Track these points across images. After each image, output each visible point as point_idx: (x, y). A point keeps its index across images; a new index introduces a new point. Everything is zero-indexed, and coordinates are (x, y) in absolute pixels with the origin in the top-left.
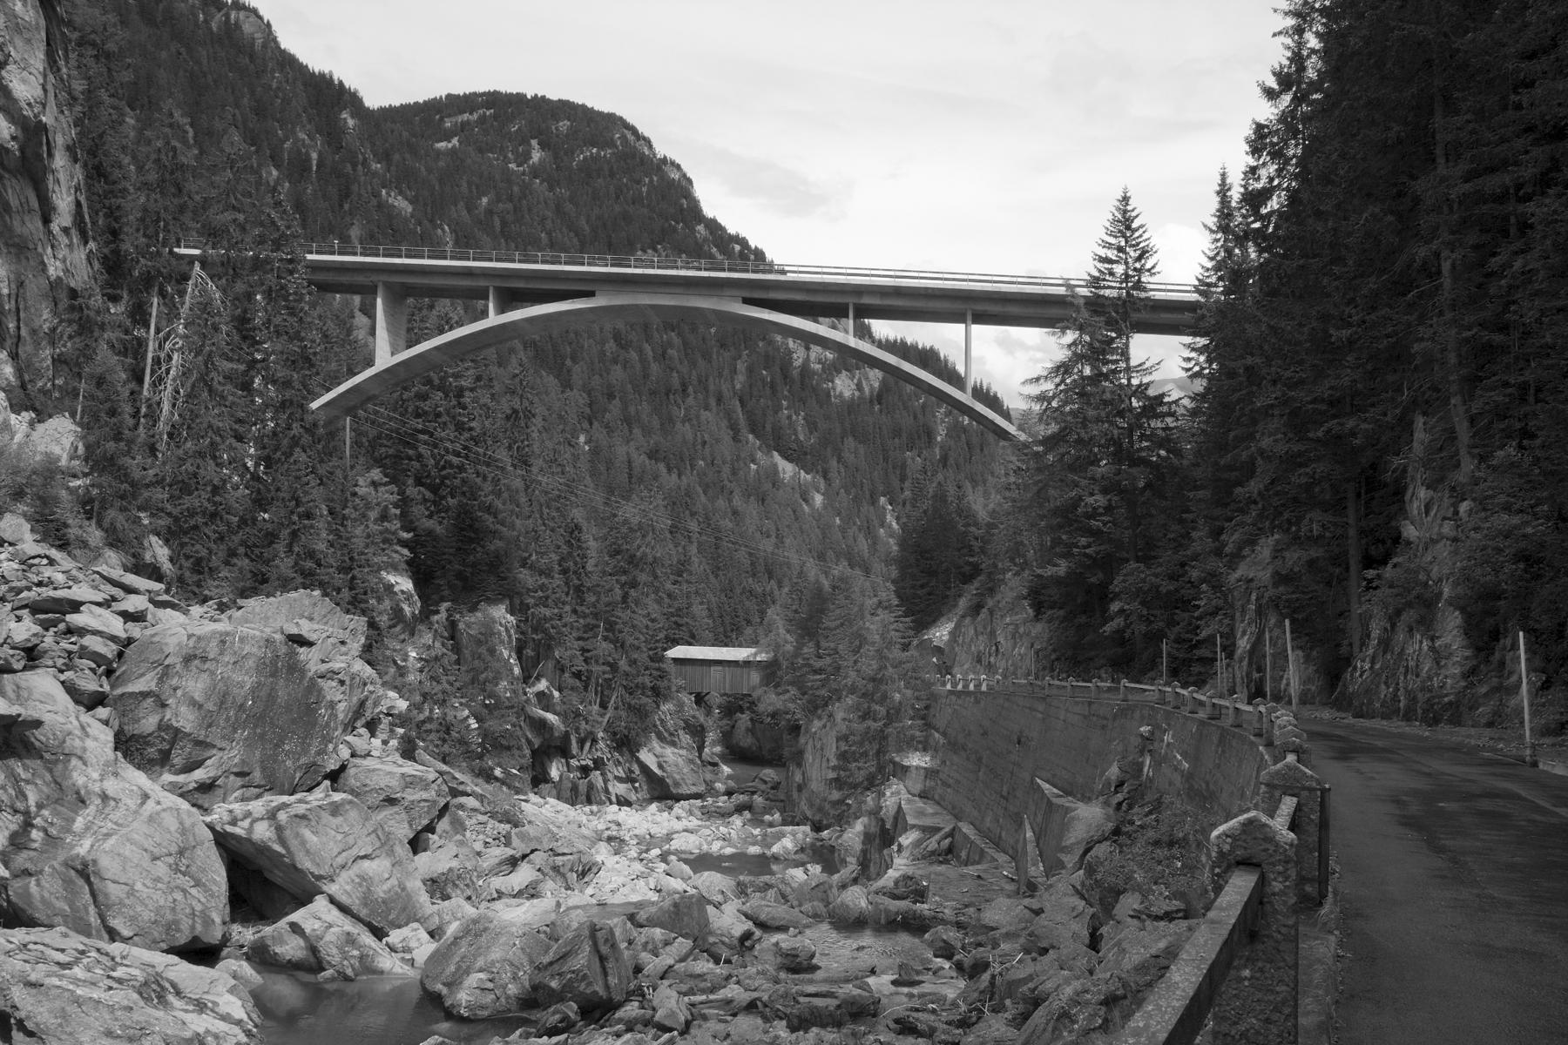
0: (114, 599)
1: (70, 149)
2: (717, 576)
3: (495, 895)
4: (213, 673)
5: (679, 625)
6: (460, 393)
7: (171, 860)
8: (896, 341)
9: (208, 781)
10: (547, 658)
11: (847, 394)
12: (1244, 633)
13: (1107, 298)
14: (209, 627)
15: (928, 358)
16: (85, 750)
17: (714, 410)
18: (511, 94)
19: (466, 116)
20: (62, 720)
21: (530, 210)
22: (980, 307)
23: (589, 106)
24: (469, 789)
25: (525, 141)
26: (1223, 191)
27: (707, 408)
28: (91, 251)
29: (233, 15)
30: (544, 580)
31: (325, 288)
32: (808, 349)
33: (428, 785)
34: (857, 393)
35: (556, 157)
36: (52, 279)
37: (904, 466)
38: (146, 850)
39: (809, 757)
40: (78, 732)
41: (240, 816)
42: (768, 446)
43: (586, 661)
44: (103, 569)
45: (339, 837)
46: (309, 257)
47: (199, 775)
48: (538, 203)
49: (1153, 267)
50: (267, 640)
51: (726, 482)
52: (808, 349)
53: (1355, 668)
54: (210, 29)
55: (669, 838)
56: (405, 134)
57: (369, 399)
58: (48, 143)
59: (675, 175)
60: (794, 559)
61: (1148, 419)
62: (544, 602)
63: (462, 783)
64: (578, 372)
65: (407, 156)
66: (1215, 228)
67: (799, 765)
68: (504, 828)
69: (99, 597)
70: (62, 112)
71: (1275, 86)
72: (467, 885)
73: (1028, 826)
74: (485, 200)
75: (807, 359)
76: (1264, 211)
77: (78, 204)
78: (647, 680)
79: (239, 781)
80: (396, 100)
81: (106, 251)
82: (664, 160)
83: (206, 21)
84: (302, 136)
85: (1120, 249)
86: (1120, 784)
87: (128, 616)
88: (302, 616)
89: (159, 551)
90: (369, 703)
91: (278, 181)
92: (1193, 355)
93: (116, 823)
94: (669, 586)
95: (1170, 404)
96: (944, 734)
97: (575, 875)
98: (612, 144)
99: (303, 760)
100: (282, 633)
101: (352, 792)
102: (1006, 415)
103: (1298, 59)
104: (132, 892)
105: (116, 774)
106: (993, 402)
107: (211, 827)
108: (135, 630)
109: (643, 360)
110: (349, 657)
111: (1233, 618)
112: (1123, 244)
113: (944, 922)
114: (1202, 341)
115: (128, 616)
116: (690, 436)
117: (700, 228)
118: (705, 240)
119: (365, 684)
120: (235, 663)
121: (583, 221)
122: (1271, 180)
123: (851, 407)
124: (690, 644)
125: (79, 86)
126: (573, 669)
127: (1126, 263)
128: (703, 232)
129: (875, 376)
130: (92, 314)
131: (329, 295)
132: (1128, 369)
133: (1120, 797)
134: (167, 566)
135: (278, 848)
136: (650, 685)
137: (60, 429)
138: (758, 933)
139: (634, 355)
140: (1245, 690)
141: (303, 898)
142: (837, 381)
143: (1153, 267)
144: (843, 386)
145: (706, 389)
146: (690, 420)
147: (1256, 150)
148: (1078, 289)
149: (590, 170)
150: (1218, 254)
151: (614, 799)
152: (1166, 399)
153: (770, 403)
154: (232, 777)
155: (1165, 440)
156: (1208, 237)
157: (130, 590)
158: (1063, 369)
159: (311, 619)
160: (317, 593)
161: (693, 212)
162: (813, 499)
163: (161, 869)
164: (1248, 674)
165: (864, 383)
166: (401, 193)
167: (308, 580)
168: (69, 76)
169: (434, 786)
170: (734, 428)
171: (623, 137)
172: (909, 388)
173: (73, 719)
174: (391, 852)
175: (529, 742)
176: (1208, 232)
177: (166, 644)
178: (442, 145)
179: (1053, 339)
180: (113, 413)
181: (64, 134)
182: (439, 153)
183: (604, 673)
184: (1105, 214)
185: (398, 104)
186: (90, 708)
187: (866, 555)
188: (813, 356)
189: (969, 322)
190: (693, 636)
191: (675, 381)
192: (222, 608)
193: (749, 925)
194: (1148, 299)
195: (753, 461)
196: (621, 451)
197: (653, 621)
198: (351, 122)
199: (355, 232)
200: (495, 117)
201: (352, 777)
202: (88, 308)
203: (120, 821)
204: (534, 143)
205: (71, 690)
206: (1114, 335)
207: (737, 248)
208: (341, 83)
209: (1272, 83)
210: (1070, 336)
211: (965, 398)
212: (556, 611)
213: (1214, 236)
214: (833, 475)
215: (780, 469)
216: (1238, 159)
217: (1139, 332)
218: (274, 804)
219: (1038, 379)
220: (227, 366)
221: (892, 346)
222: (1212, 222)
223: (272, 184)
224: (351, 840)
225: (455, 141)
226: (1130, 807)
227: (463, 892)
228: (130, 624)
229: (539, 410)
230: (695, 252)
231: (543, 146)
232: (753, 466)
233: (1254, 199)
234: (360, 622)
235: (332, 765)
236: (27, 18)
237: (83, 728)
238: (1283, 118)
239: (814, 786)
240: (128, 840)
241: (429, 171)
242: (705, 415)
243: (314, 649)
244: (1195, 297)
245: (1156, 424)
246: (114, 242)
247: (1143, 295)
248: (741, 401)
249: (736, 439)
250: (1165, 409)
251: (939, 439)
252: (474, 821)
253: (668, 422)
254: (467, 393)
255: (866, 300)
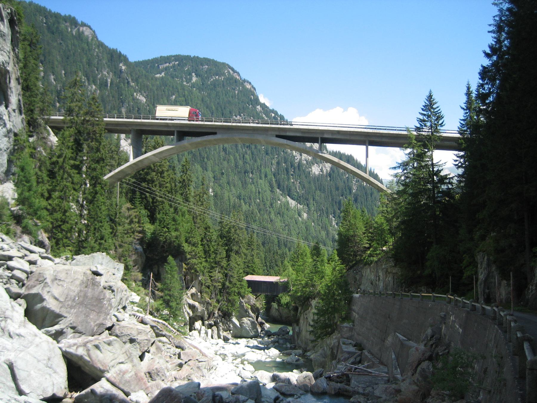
0: (26, 256)
1: (17, 79)
2: (264, 247)
3: (174, 379)
4: (62, 286)
5: (248, 267)
6: (162, 173)
7: (45, 362)
8: (336, 152)
9: (60, 330)
10: (196, 279)
11: (317, 173)
12: (482, 273)
13: (424, 135)
14: (61, 267)
15: (349, 159)
16: (13, 316)
17: (264, 180)
18: (185, 56)
19: (167, 64)
20: (4, 304)
21: (191, 100)
22: (372, 139)
23: (215, 60)
24: (164, 333)
25: (190, 74)
26: (469, 94)
27: (261, 178)
28: (23, 118)
29: (81, 29)
30: (194, 248)
31: (111, 131)
32: (301, 155)
33: (147, 333)
34: (321, 173)
35: (202, 79)
36: (8, 129)
37: (340, 203)
38: (35, 358)
39: (301, 321)
40: (10, 309)
41: (72, 345)
42: (285, 194)
43: (211, 281)
44: (23, 244)
45: (111, 354)
46: (105, 119)
47: (57, 327)
48: (195, 98)
49: (442, 123)
50: (84, 273)
51: (268, 208)
52: (301, 155)
53: (529, 288)
54: (73, 34)
55: (244, 355)
56: (144, 72)
57: (127, 175)
58: (9, 78)
59: (248, 86)
60: (295, 240)
61: (441, 184)
62: (194, 257)
63: (161, 331)
64: (210, 164)
65: (145, 80)
66: (465, 108)
67: (298, 325)
68: (178, 351)
69: (20, 255)
70: (15, 66)
71: (489, 52)
72: (163, 375)
73: (393, 353)
74: (174, 97)
75: (301, 159)
76: (487, 101)
77: (19, 101)
78: (236, 289)
79: (72, 331)
80: (141, 58)
81: (29, 118)
82: (244, 81)
83: (71, 31)
84: (105, 73)
85: (429, 116)
86: (432, 337)
87: (31, 263)
88: (98, 263)
89: (43, 236)
90: (124, 299)
91: (95, 90)
92: (458, 159)
93: (24, 346)
94: (245, 251)
95: (450, 178)
96: (358, 314)
97: (206, 370)
98: (224, 74)
99: (98, 322)
100: (90, 270)
101: (117, 336)
102: (381, 182)
103: (499, 41)
104: (29, 375)
105: (25, 326)
106: (376, 177)
107: (60, 348)
108: (33, 268)
109: (235, 159)
110: (116, 280)
111: (477, 267)
112: (430, 114)
113: (358, 393)
114: (462, 153)
115: (31, 263)
116: (254, 189)
117: (259, 107)
118: (261, 112)
119: (122, 291)
120: (72, 282)
121: (212, 104)
122: (490, 89)
123: (318, 179)
124: (253, 274)
125: (21, 56)
126: (206, 284)
127: (431, 121)
128: (259, 109)
129: (328, 166)
130: (22, 142)
131: (113, 134)
132: (433, 165)
133: (431, 342)
134: (47, 242)
135: (87, 358)
136: (237, 291)
137: (9, 187)
138: (281, 397)
139: (232, 157)
140: (483, 297)
141: (96, 379)
142: (313, 168)
143: (442, 123)
144: (315, 170)
145: (260, 171)
146: (253, 183)
147: (482, 78)
148: (412, 132)
149: (215, 85)
150: (467, 118)
151: (222, 337)
152: (448, 177)
153: (286, 177)
154: (69, 329)
155: (448, 193)
156: (463, 112)
157: (32, 252)
158: (404, 165)
159: (102, 264)
160: (104, 254)
161: (256, 101)
162: (303, 215)
163: (41, 366)
164: (484, 291)
165: (324, 169)
166: (141, 94)
167: (102, 249)
168: (18, 52)
169: (149, 333)
170: (271, 186)
171: (229, 72)
172: (342, 171)
173: (9, 303)
174: (132, 361)
175: (188, 314)
176: (463, 110)
177: (45, 274)
178: (158, 75)
179: (402, 151)
180: (28, 181)
181: (15, 74)
182: (156, 78)
183: (219, 286)
184: (422, 101)
185: (141, 60)
186: (15, 299)
187: (324, 237)
188: (303, 158)
189: (367, 145)
190: (254, 271)
191: (248, 168)
192: (67, 259)
193: (278, 394)
194: (441, 136)
195: (279, 200)
196: (226, 195)
197: (239, 265)
198: (123, 68)
199: (123, 110)
200: (179, 65)
201: (117, 330)
202: (21, 140)
203: (26, 346)
204: (193, 74)
205: (8, 291)
206: (426, 150)
207: (273, 115)
208: (120, 52)
209: (488, 51)
210: (409, 150)
211: (366, 176)
212: (200, 261)
213: (465, 111)
214: (311, 206)
215: (290, 203)
216: (475, 81)
217: (437, 149)
218: (86, 340)
219: (395, 168)
220: (72, 162)
221: (335, 154)
222: (464, 106)
223: (93, 91)
224: (116, 356)
225: (163, 74)
226: (436, 346)
227: (161, 378)
228: (32, 265)
229: (194, 179)
230: (257, 117)
231: (197, 75)
232: (279, 202)
233: (482, 97)
234: (122, 266)
235: (109, 324)
236: (5, 32)
237: (12, 307)
238: (493, 65)
239: (304, 333)
240: (29, 353)
241: (153, 85)
242: (260, 181)
243: (102, 277)
244: (458, 135)
245: (444, 187)
246: (32, 114)
247: (438, 135)
248: (274, 175)
249: (272, 191)
250: (447, 181)
251: (354, 191)
252: (166, 347)
253: (244, 184)
254: (165, 172)
255: (326, 136)
